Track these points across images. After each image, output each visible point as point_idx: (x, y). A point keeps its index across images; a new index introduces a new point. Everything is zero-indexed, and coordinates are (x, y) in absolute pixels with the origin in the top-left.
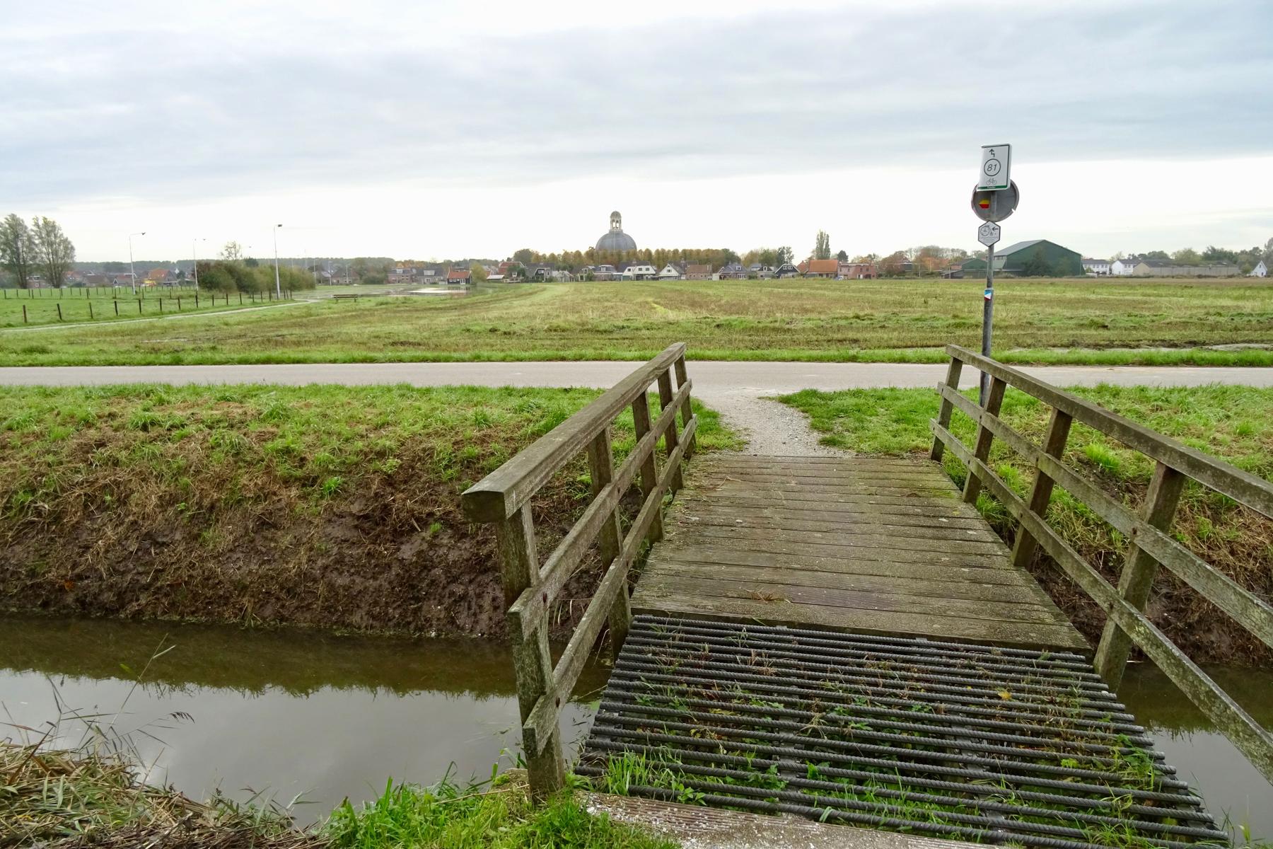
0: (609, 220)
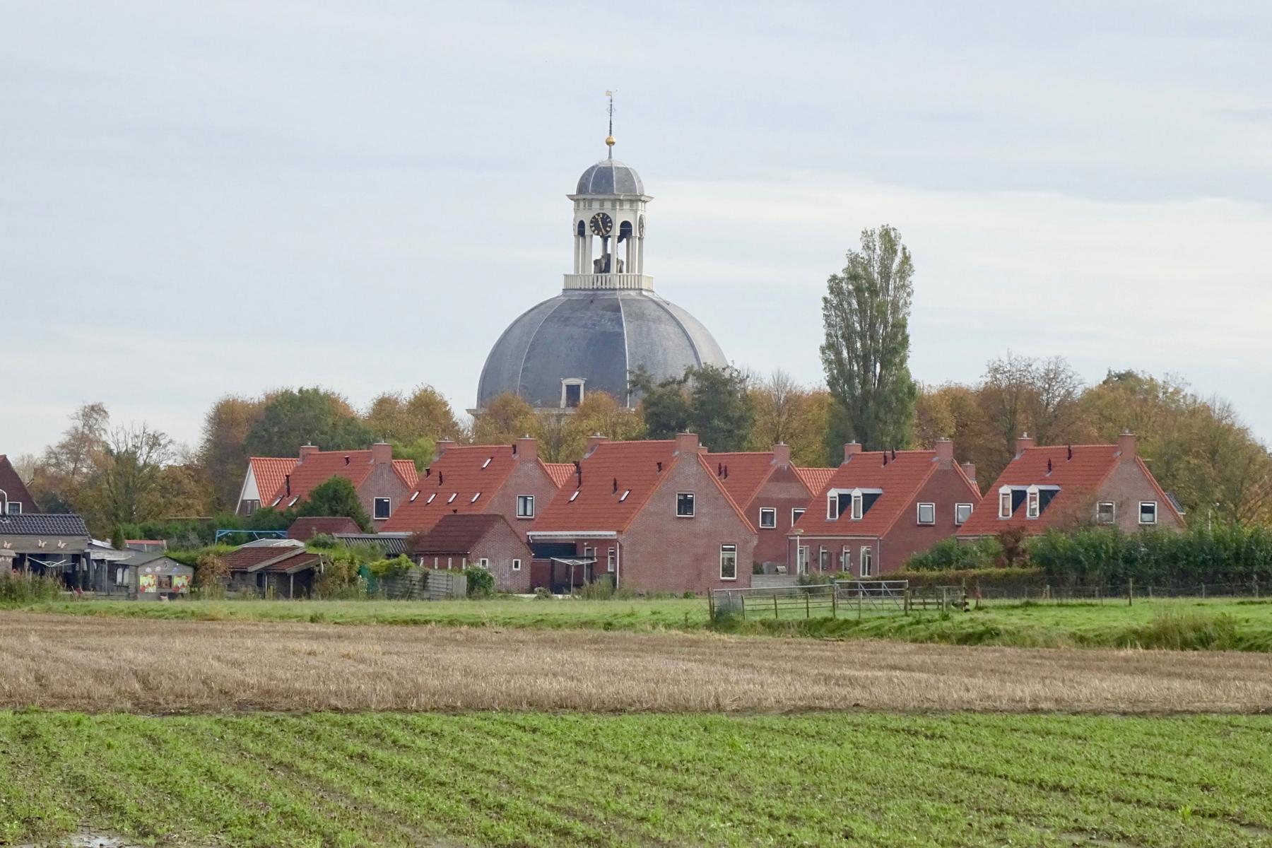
0: (566, 215)
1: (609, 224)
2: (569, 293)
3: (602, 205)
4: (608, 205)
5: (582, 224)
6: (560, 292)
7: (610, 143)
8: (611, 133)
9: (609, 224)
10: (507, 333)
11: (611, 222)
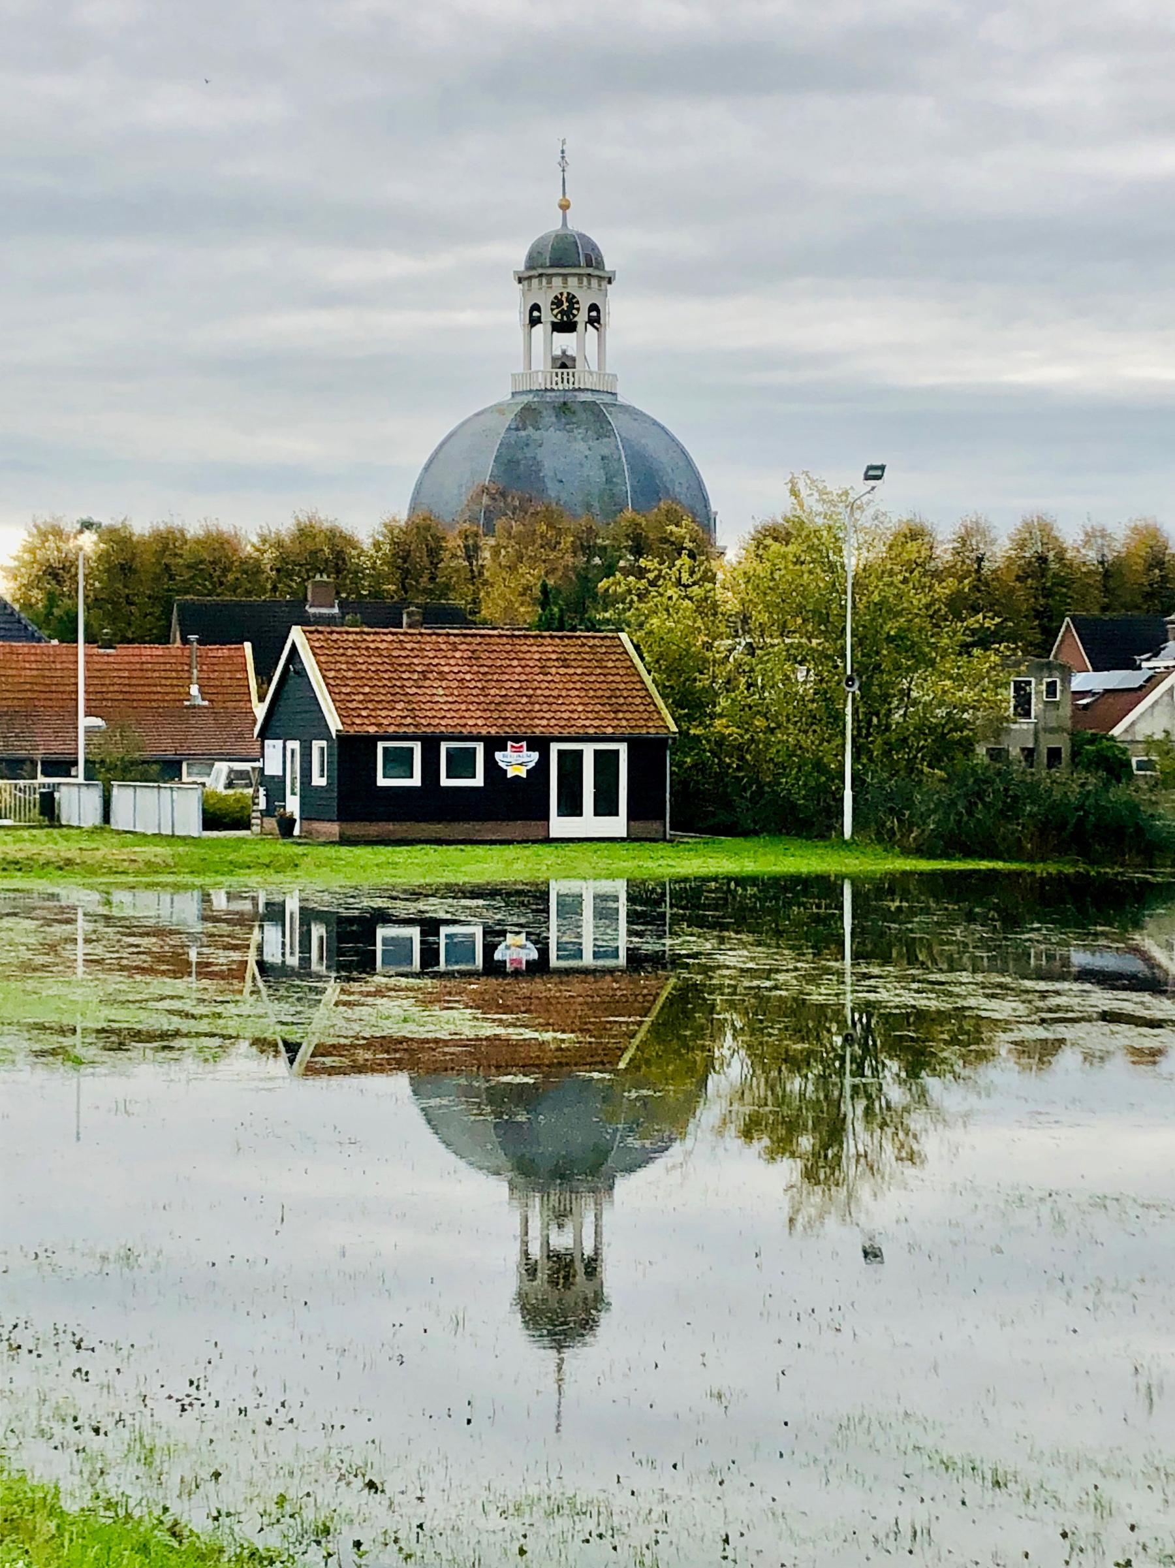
3: (565, 282)
4: (573, 281)
8: (564, 193)
11: (577, 302)
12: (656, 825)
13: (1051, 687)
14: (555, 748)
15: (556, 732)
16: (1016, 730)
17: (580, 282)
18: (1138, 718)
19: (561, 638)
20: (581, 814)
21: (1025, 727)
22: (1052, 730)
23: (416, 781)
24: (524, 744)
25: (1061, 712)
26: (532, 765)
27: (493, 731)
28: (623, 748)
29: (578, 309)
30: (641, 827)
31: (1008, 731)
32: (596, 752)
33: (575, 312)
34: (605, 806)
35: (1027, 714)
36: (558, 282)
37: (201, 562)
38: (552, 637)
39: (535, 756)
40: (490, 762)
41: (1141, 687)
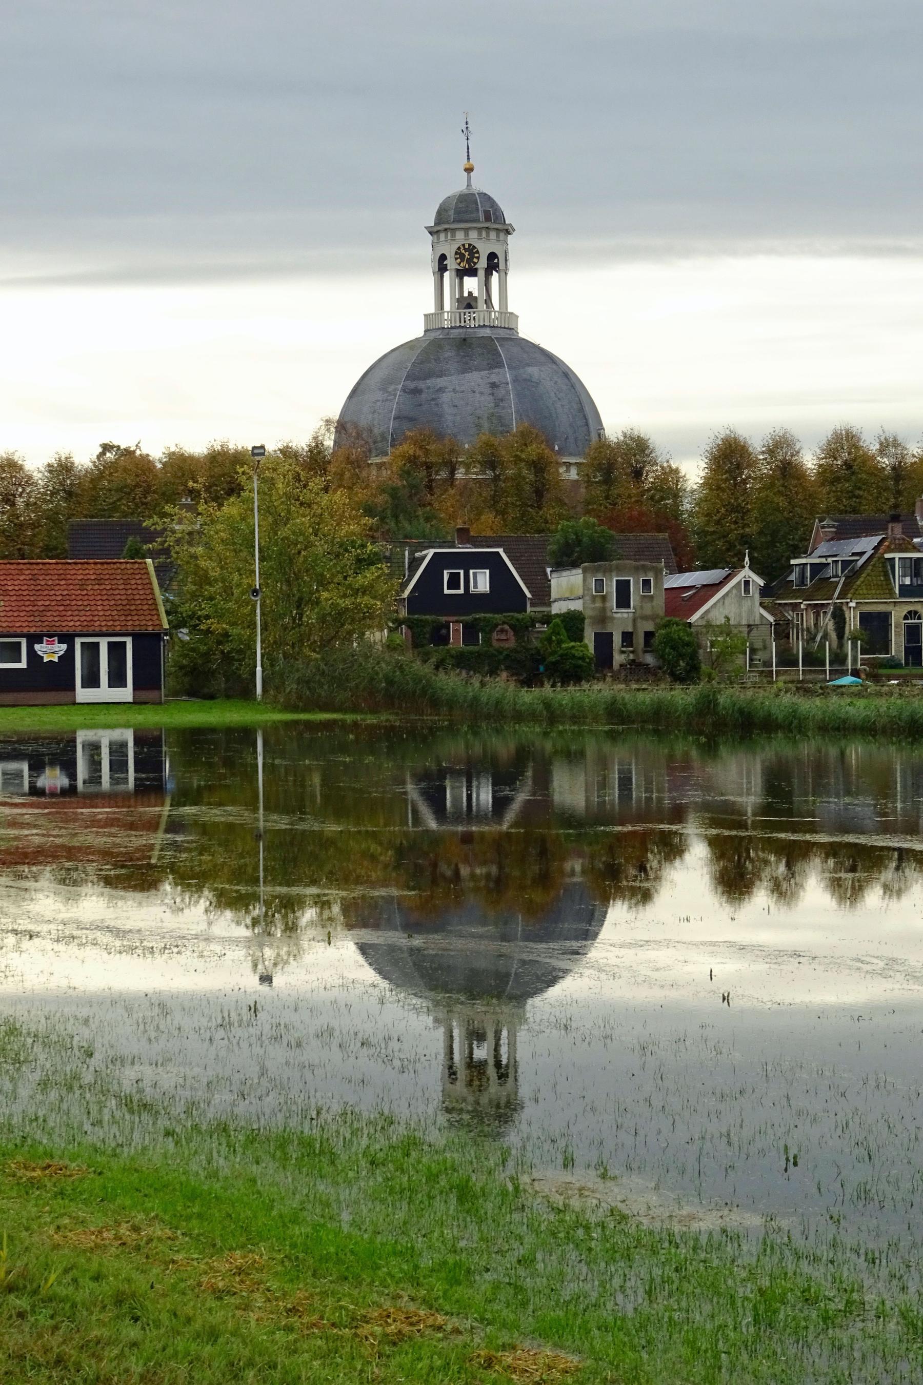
1: (476, 255)
2: (428, 334)
3: (467, 235)
4: (473, 235)
5: (443, 257)
6: (420, 333)
7: (469, 170)
8: (469, 159)
9: (476, 255)
10: (550, 359)
11: (477, 252)
12: (156, 693)
13: (646, 583)
14: (78, 641)
15: (78, 630)
16: (619, 619)
17: (480, 234)
18: (712, 607)
19: (102, 564)
20: (99, 687)
21: (625, 615)
22: (645, 618)
23: (471, 572)
24: (56, 638)
25: (655, 603)
26: (62, 653)
27: (32, 630)
28: (129, 641)
29: (478, 258)
30: (145, 695)
31: (613, 619)
32: (109, 643)
33: (475, 260)
34: (117, 679)
35: (628, 606)
36: (460, 235)
37: (126, 486)
38: (95, 563)
39: (64, 647)
40: (31, 652)
41: (721, 582)
